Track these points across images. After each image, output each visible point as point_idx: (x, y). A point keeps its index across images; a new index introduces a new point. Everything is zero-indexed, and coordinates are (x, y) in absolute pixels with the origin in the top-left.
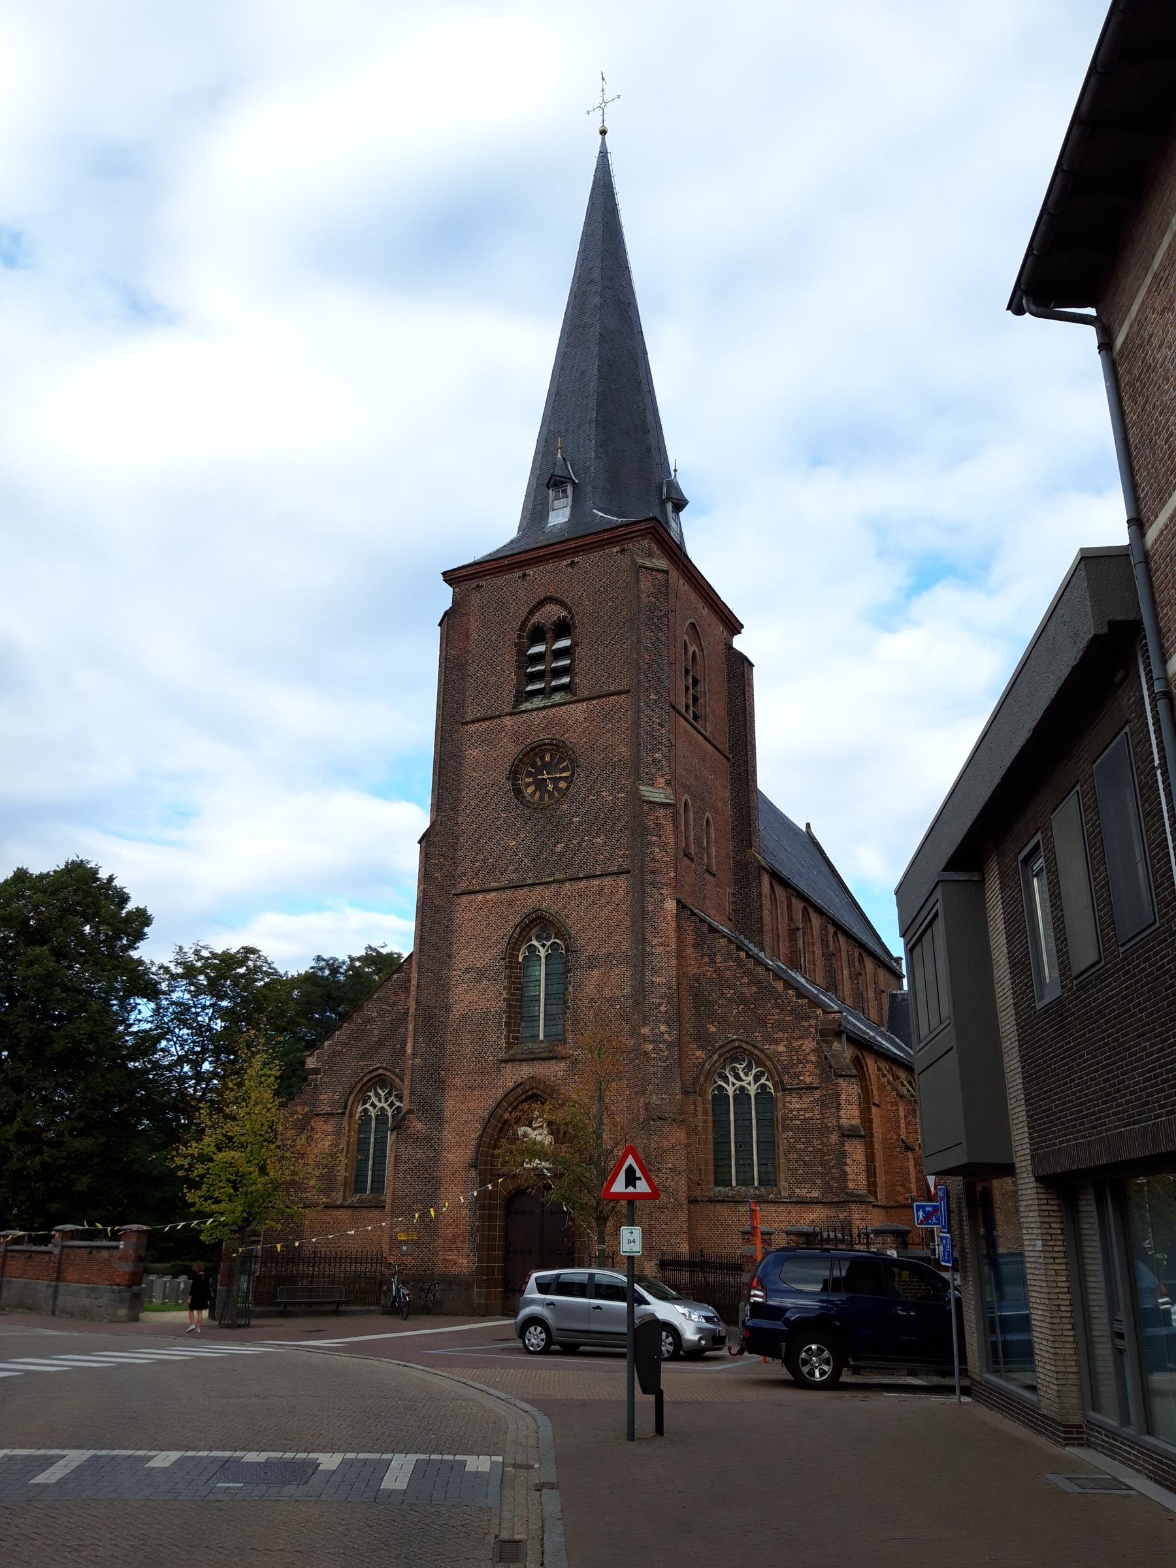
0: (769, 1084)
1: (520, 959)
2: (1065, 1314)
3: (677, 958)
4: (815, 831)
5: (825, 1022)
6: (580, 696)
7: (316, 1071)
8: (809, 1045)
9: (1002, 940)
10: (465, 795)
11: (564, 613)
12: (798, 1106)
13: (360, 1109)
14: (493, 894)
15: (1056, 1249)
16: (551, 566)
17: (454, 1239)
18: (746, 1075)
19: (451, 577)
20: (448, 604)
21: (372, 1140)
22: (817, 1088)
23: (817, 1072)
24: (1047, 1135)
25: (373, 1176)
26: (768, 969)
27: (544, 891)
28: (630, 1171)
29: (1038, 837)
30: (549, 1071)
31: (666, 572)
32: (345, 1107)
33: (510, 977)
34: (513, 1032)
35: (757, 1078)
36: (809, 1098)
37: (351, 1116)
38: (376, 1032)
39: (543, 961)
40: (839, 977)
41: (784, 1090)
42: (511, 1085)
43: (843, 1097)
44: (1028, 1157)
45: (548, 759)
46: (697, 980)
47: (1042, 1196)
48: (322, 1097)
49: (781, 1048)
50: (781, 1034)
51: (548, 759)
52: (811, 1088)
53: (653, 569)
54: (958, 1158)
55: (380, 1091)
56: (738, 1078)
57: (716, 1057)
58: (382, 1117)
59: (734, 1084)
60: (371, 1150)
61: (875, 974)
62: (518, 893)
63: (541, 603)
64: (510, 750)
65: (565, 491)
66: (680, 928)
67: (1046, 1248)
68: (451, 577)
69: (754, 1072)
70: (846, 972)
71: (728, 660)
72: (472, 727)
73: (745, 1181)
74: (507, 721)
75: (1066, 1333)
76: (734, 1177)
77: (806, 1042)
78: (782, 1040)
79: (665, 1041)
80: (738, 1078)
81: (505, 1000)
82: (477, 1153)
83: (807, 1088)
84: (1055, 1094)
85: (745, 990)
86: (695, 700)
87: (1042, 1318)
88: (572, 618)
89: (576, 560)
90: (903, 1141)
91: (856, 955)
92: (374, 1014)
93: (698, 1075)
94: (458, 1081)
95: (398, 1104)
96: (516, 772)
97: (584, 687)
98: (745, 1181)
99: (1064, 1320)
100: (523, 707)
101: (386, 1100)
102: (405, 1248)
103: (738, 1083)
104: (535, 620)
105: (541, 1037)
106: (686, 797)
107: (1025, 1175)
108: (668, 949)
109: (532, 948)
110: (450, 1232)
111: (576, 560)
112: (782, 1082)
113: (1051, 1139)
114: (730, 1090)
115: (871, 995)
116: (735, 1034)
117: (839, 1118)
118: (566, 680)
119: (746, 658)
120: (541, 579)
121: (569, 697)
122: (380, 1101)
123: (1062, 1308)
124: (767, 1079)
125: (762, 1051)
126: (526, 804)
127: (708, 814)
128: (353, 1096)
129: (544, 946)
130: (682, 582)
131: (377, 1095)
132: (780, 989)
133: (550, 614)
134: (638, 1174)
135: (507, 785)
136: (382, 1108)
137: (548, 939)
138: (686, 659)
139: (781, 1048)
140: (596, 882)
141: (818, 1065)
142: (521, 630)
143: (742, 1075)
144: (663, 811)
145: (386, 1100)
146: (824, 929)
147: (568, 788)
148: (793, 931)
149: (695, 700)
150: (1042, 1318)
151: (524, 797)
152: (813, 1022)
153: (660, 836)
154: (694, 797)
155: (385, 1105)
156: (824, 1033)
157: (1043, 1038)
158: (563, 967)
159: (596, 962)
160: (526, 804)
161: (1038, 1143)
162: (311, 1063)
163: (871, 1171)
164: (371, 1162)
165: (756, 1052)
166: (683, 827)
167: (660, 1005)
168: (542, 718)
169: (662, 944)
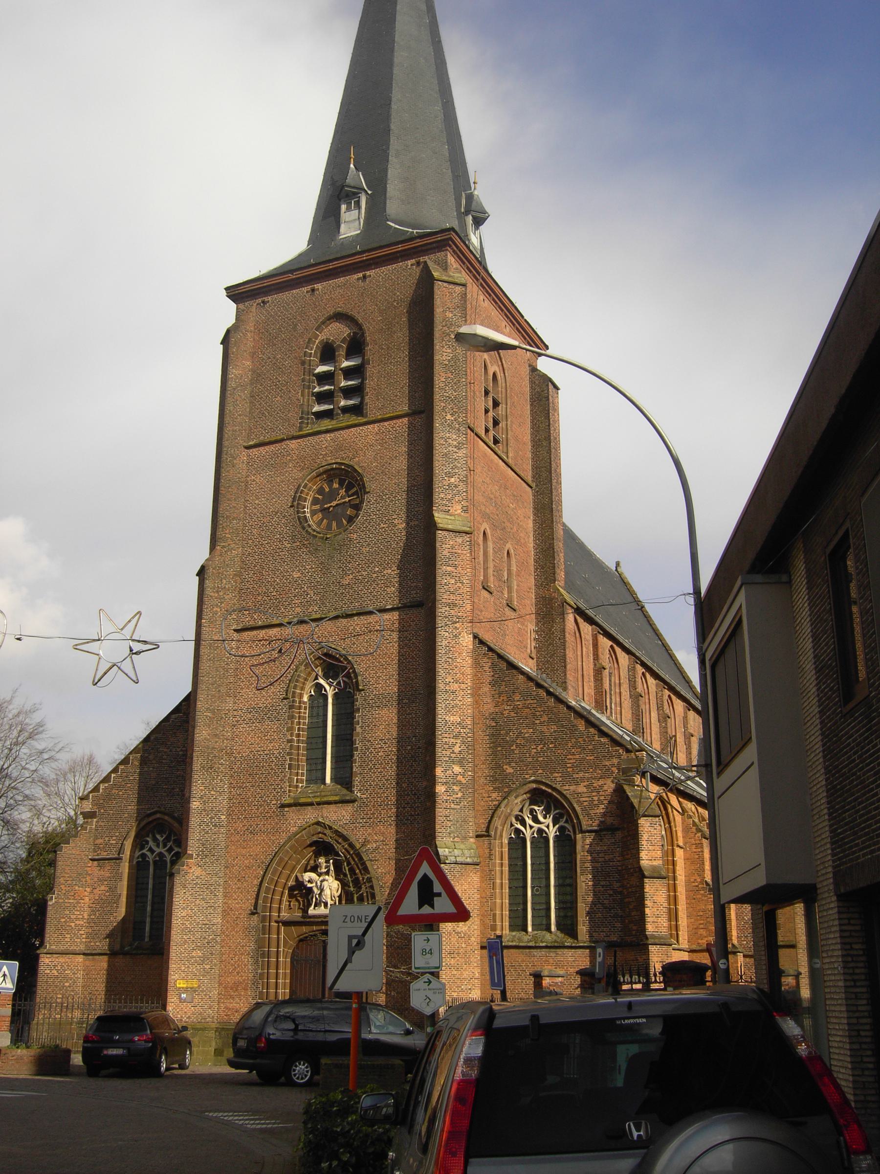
0: (566, 825)
2: (865, 1040)
3: (472, 695)
4: (622, 569)
6: (371, 417)
9: (809, 645)
15: (857, 971)
19: (236, 293)
20: (231, 320)
21: (150, 886)
22: (617, 829)
24: (851, 848)
25: (152, 923)
29: (848, 524)
30: (337, 816)
31: (464, 285)
40: (646, 720)
41: (582, 832)
44: (831, 875)
46: (493, 719)
47: (845, 916)
49: (581, 789)
50: (581, 775)
54: (758, 880)
55: (158, 837)
59: (531, 827)
60: (150, 897)
61: (685, 718)
66: (477, 664)
67: (847, 971)
68: (236, 293)
70: (654, 715)
71: (532, 382)
75: (865, 1059)
78: (583, 780)
79: (460, 783)
80: (536, 820)
84: (859, 804)
86: (496, 423)
87: (841, 1045)
88: (363, 334)
89: (368, 273)
91: (666, 697)
95: (176, 849)
99: (864, 1046)
101: (165, 846)
102: (184, 996)
106: (485, 526)
107: (826, 895)
113: (855, 852)
114: (528, 834)
115: (680, 739)
120: (334, 293)
122: (158, 846)
123: (862, 1033)
124: (566, 822)
127: (509, 546)
130: (482, 297)
131: (155, 840)
136: (161, 855)
138: (486, 380)
139: (581, 789)
143: (541, 818)
146: (632, 670)
148: (599, 671)
149: (496, 423)
150: (841, 1045)
153: (456, 566)
154: (494, 527)
157: (849, 744)
161: (839, 859)
163: (673, 915)
164: (149, 908)
166: (481, 559)
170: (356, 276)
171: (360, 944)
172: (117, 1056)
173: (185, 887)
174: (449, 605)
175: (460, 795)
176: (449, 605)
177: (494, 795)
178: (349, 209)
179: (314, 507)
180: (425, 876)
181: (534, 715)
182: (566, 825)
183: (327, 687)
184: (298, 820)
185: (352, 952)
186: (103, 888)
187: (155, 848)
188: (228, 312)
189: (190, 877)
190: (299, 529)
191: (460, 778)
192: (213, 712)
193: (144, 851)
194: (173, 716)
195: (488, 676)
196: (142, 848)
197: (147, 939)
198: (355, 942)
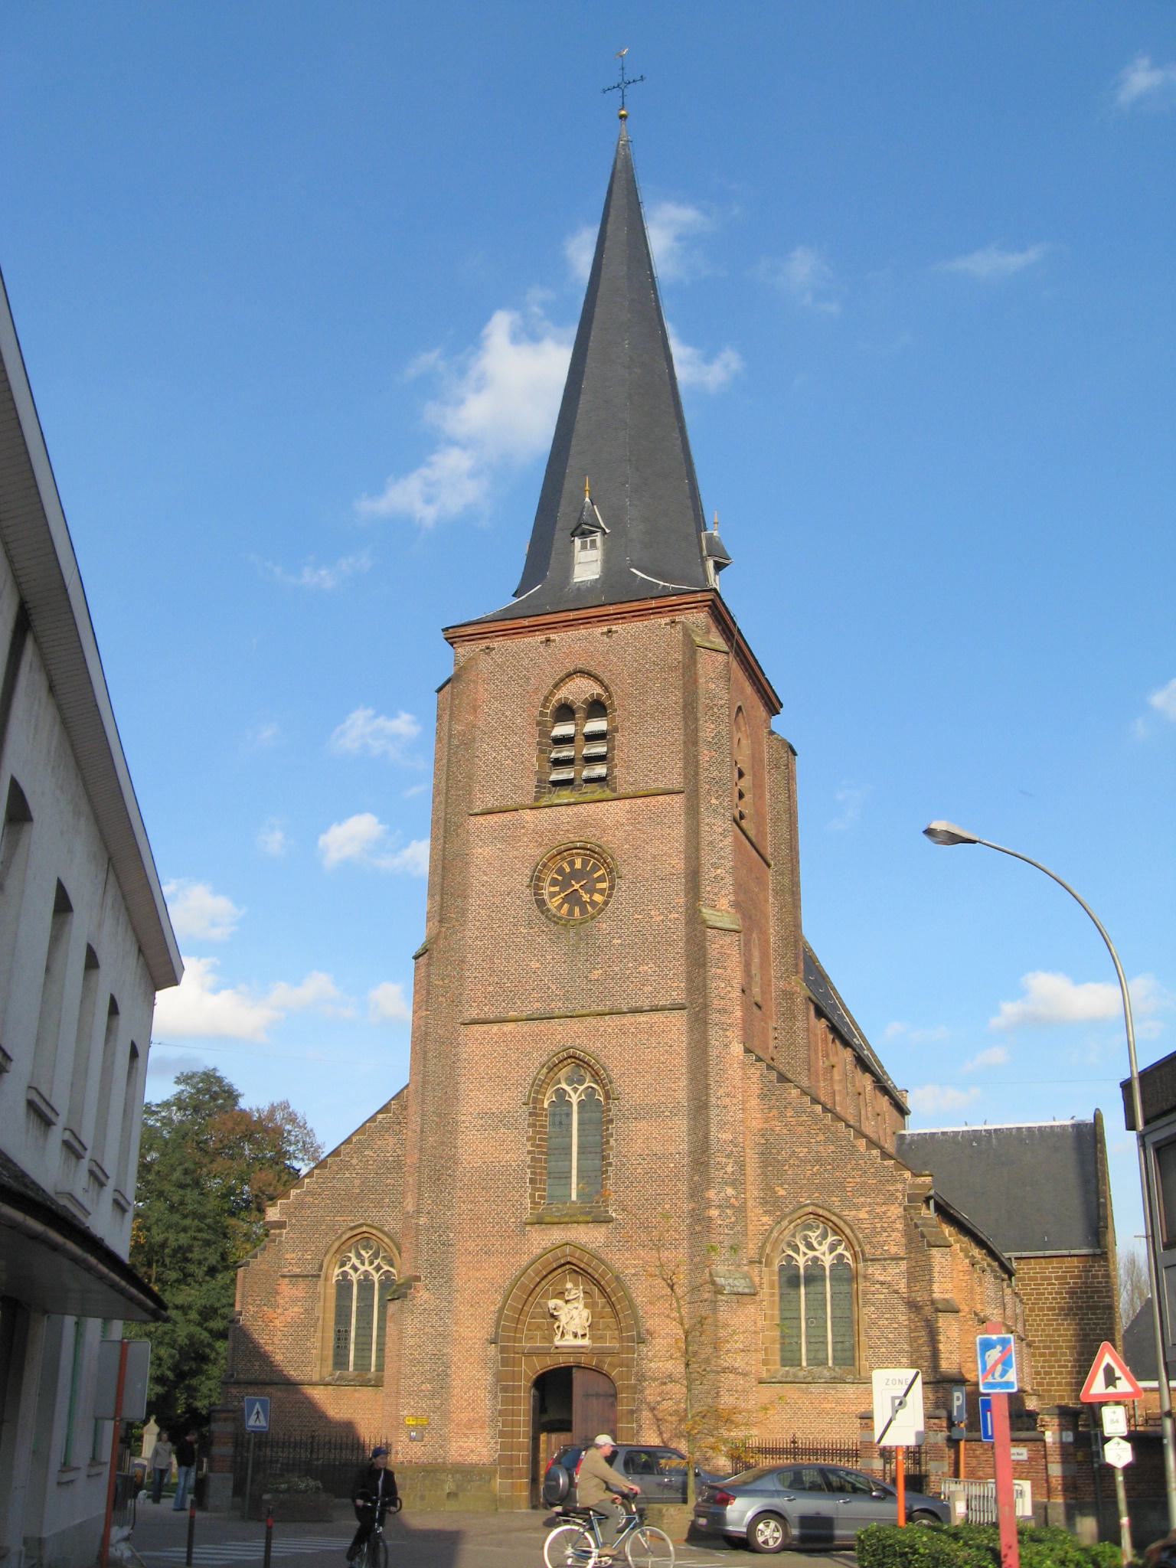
0: (845, 1253)
1: (546, 1105)
5: (914, 1186)
7: (280, 1225)
8: (896, 1211)
10: (474, 903)
11: (597, 690)
13: (337, 1271)
14: (511, 1025)
16: (583, 631)
17: (470, 1425)
18: (820, 1244)
22: (903, 1259)
23: (903, 1241)
26: (848, 1126)
27: (575, 1025)
30: (590, 1236)
33: (534, 1126)
34: (538, 1190)
37: (326, 1279)
38: (357, 1182)
39: (575, 1108)
41: (865, 1260)
43: (937, 1269)
45: (578, 865)
48: (288, 1256)
49: (863, 1215)
50: (862, 1199)
52: (896, 1259)
56: (810, 1247)
57: (785, 1223)
58: (366, 1285)
59: (805, 1254)
62: (543, 1026)
65: (593, 542)
72: (481, 819)
73: (818, 1361)
74: (528, 815)
76: (804, 1357)
77: (892, 1208)
78: (863, 1205)
80: (810, 1247)
82: (497, 1327)
83: (892, 1259)
88: (610, 697)
93: (764, 1244)
95: (386, 1268)
96: (539, 879)
98: (818, 1361)
101: (371, 1263)
103: (811, 1254)
105: (574, 1197)
108: (735, 1101)
109: (561, 1094)
110: (464, 1417)
111: (614, 628)
116: (809, 1197)
117: (931, 1292)
118: (600, 770)
121: (608, 794)
122: (363, 1264)
124: (846, 1249)
126: (554, 920)
128: (328, 1257)
129: (575, 1090)
131: (359, 1256)
132: (862, 1149)
133: (580, 690)
134: (1118, 1373)
137: (581, 1082)
140: (642, 1018)
141: (907, 1234)
142: (544, 706)
143: (815, 1244)
145: (371, 1263)
147: (606, 903)
151: (548, 910)
152: (900, 1186)
153: (725, 968)
155: (370, 1269)
156: (912, 1198)
158: (599, 1118)
159: (641, 1113)
160: (554, 920)
167: (727, 1165)
168: (565, 818)
169: (728, 1095)
170: (600, 630)
173: (412, 1313)
175: (733, 1219)
177: (765, 1219)
178: (584, 547)
179: (552, 889)
181: (809, 1133)
182: (845, 1253)
183: (572, 1093)
184: (542, 1240)
186: (296, 1309)
187: (358, 1265)
188: (444, 661)
189: (417, 1301)
190: (537, 912)
191: (733, 1200)
192: (439, 1115)
193: (346, 1268)
194: (380, 1116)
195: (755, 1089)
196: (343, 1265)
197: (351, 1369)
198: (897, 1402)
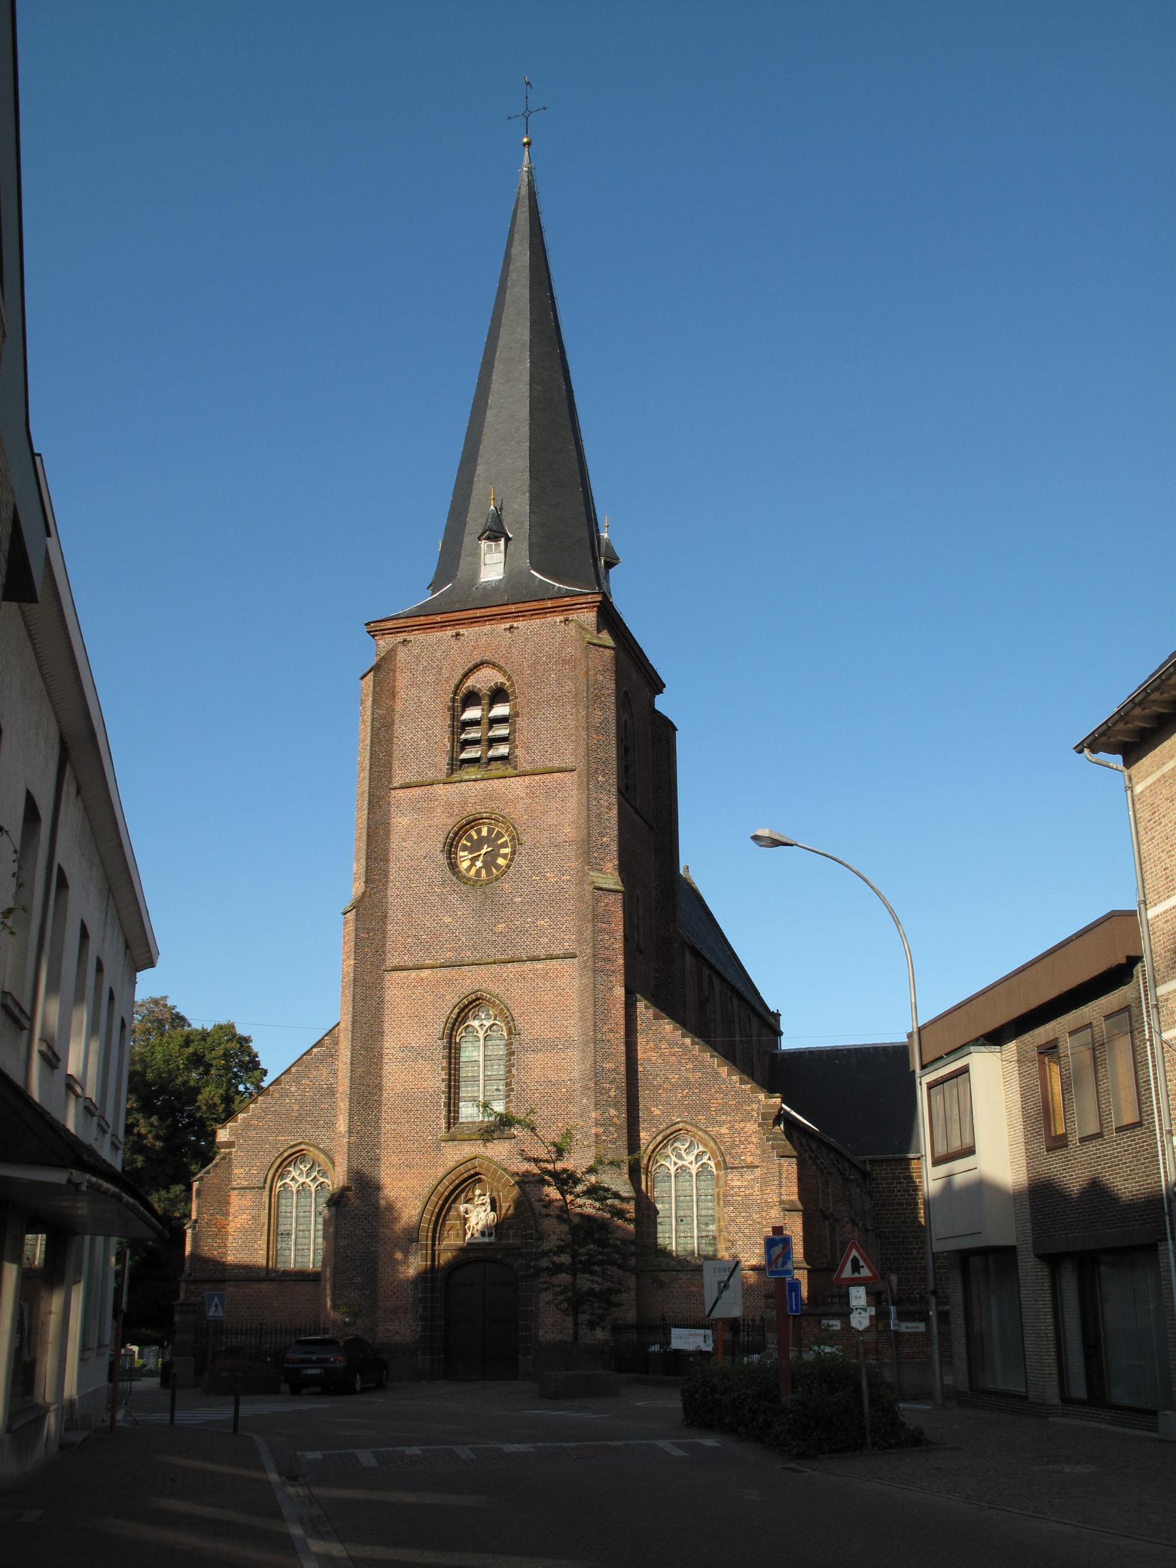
5: (767, 1106)
6: (520, 769)
7: (230, 1145)
12: (738, 1183)
16: (487, 628)
27: (483, 971)
28: (855, 1262)
32: (265, 1182)
35: (698, 1157)
36: (749, 1176)
41: (726, 1168)
42: (451, 1164)
49: (724, 1130)
50: (724, 1117)
51: (484, 832)
52: (752, 1167)
53: (600, 646)
63: (477, 667)
64: (445, 822)
69: (696, 1152)
74: (439, 789)
77: (749, 1125)
80: (680, 1157)
81: (443, 1080)
83: (748, 1167)
85: (690, 1075)
88: (512, 685)
90: (821, 1211)
92: (293, 1089)
94: (394, 1159)
95: (322, 1180)
97: (525, 766)
100: (456, 777)
101: (308, 1175)
104: (470, 682)
108: (617, 1036)
111: (515, 625)
112: (724, 1161)
119: (671, 723)
121: (510, 771)
125: (706, 1132)
133: (485, 679)
134: (862, 1263)
135: (442, 859)
139: (724, 1130)
140: (539, 965)
142: (455, 693)
143: (684, 1154)
144: (612, 897)
147: (508, 866)
151: (460, 872)
152: (755, 1106)
153: (610, 923)
162: (223, 1135)
165: (700, 1133)
167: (610, 1090)
169: (611, 1031)
170: (503, 626)
171: (726, 1286)
172: (314, 1375)
174: (604, 960)
176: (604, 960)
180: (855, 1257)
185: (721, 1292)
193: (287, 1181)
